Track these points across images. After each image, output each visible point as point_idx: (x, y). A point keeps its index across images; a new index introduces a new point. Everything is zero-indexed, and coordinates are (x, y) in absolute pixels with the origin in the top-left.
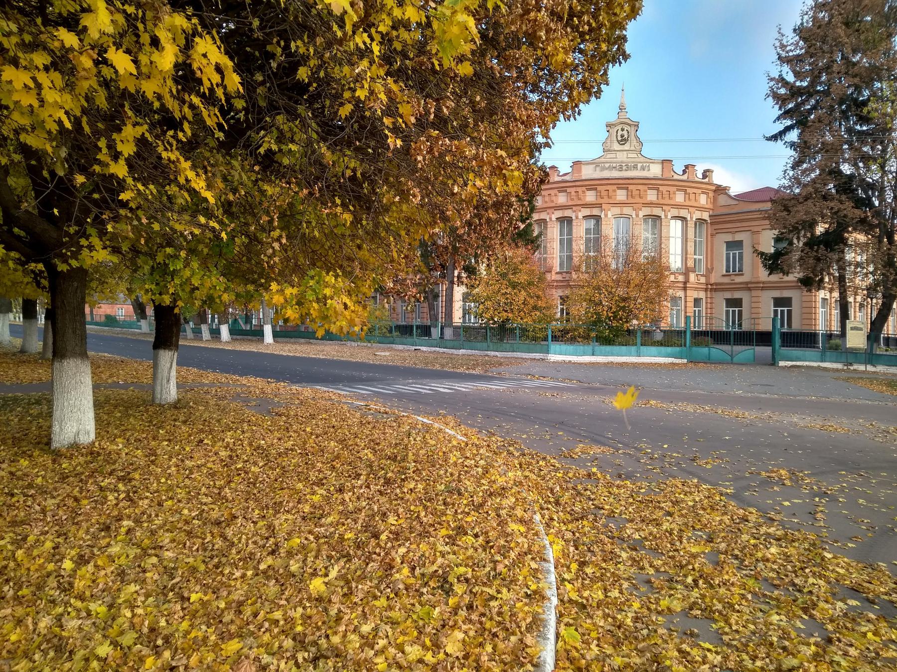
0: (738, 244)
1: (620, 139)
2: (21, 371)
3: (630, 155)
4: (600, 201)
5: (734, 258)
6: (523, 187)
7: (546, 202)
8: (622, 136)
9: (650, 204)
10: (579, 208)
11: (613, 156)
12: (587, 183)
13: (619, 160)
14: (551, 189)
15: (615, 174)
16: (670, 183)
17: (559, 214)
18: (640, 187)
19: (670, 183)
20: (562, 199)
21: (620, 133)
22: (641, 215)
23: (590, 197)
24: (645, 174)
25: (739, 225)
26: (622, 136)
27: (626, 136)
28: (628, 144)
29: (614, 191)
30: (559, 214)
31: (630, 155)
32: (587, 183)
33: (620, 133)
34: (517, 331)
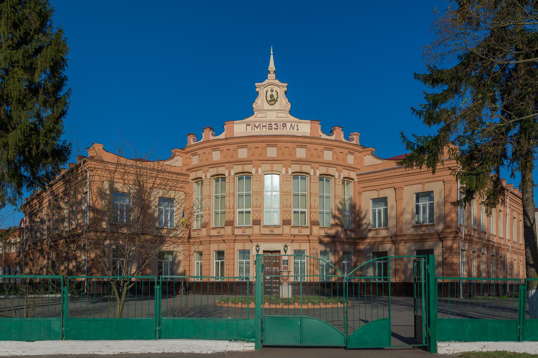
0: (384, 200)
1: (269, 99)
2: (128, 161)
3: (279, 115)
4: (252, 158)
5: (379, 213)
6: (4, 205)
7: (312, 156)
8: (272, 96)
9: (300, 161)
10: (231, 165)
11: (264, 115)
12: (237, 140)
13: (269, 118)
14: (205, 148)
15: (265, 131)
16: (317, 141)
17: (213, 171)
18: (288, 145)
19: (317, 141)
20: (216, 156)
21: (269, 93)
22: (290, 172)
23: (243, 154)
24: (294, 132)
25: (383, 182)
26: (272, 96)
27: (275, 96)
28: (278, 103)
29: (210, 153)
30: (213, 171)
31: (279, 115)
32: (237, 140)
33: (269, 93)
34: (157, 287)
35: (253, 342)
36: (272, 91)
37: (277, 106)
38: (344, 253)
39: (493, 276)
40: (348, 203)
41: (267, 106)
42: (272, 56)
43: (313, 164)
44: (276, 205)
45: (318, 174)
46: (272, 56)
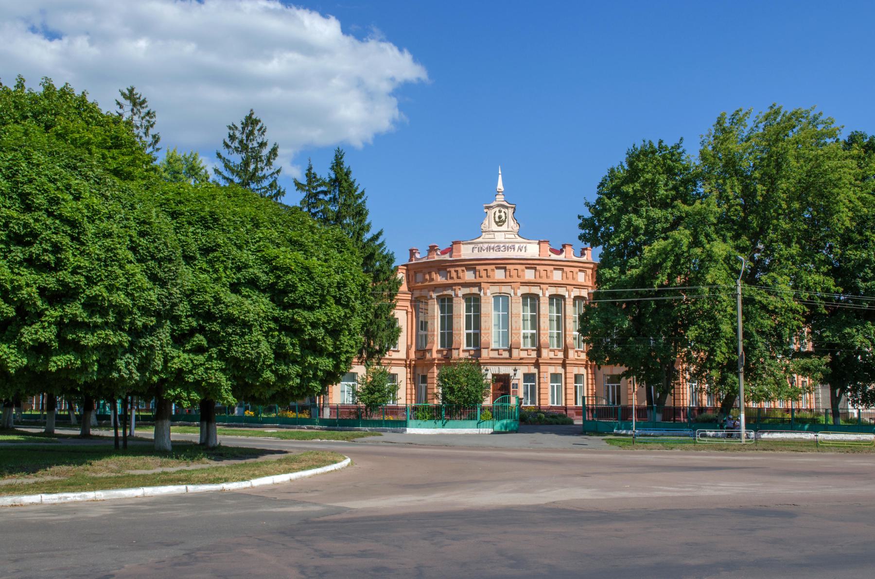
1: (497, 220)
3: (507, 236)
8: (500, 217)
11: (492, 236)
26: (500, 217)
27: (503, 218)
31: (507, 236)
33: (497, 214)
35: (198, 426)
36: (500, 212)
37: (504, 227)
38: (247, 383)
39: (547, 388)
40: (795, 168)
41: (494, 227)
42: (500, 176)
43: (542, 286)
44: (586, 491)
45: (547, 295)
46: (500, 176)
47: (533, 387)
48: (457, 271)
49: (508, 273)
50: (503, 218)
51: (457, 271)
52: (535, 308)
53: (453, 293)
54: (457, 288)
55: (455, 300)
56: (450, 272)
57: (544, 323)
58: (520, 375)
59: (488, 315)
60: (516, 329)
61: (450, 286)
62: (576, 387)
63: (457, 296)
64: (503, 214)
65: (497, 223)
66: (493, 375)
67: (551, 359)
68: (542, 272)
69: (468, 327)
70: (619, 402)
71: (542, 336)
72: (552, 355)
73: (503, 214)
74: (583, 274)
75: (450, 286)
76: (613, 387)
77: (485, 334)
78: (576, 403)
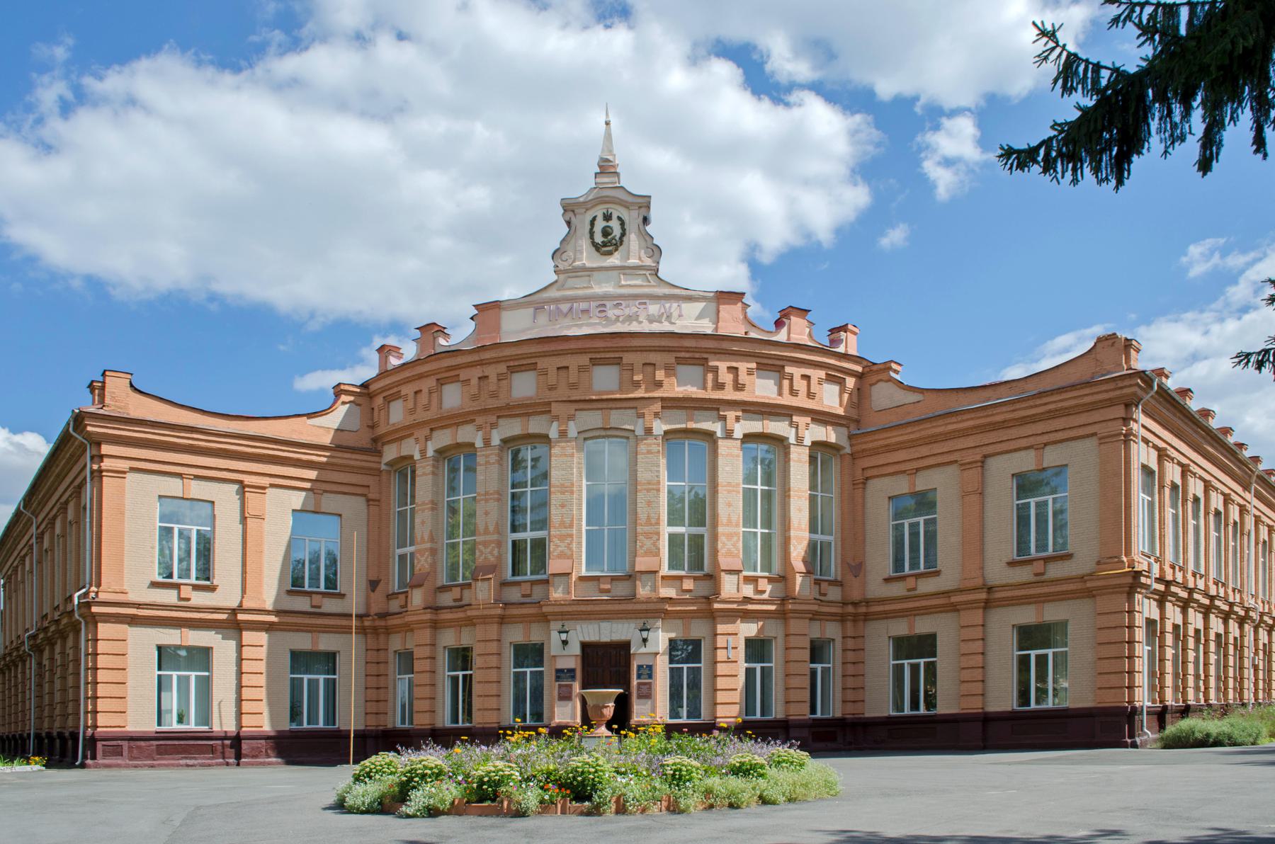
1: (599, 238)
8: (606, 232)
27: (617, 232)
33: (600, 224)
36: (607, 217)
47: (695, 674)
48: (733, 370)
49: (786, 383)
50: (617, 232)
51: (733, 370)
52: (776, 473)
53: (717, 428)
54: (731, 415)
55: (724, 446)
56: (715, 370)
57: (730, 507)
58: (660, 639)
59: (568, 489)
60: (648, 522)
61: (714, 407)
62: (813, 673)
63: (729, 435)
64: (614, 224)
65: (597, 247)
66: (585, 646)
67: (747, 600)
68: (797, 378)
69: (749, 520)
70: (930, 703)
71: (722, 540)
72: (748, 591)
73: (614, 224)
74: (836, 388)
75: (714, 407)
76: (915, 668)
77: (648, 535)
78: (813, 711)
